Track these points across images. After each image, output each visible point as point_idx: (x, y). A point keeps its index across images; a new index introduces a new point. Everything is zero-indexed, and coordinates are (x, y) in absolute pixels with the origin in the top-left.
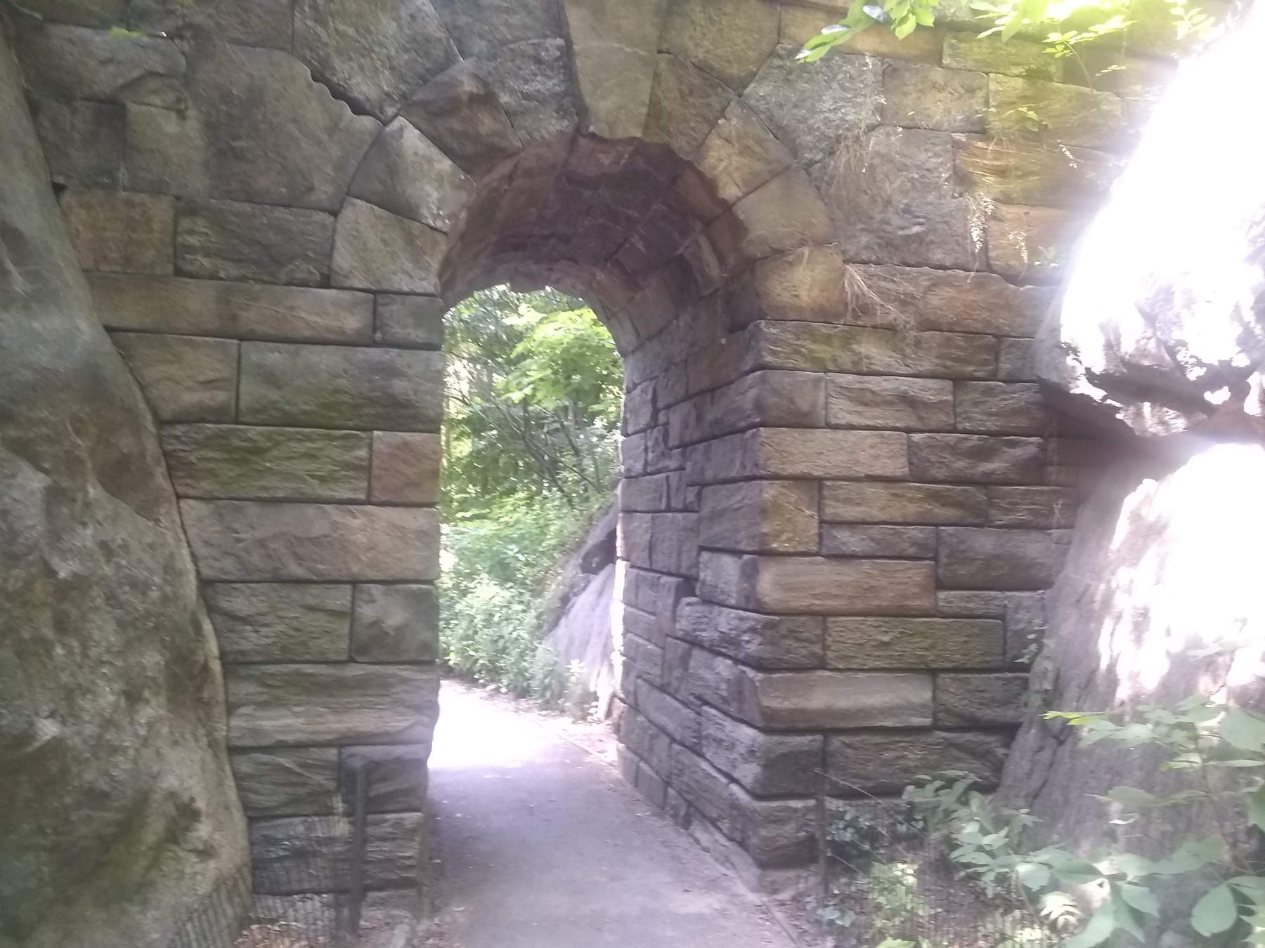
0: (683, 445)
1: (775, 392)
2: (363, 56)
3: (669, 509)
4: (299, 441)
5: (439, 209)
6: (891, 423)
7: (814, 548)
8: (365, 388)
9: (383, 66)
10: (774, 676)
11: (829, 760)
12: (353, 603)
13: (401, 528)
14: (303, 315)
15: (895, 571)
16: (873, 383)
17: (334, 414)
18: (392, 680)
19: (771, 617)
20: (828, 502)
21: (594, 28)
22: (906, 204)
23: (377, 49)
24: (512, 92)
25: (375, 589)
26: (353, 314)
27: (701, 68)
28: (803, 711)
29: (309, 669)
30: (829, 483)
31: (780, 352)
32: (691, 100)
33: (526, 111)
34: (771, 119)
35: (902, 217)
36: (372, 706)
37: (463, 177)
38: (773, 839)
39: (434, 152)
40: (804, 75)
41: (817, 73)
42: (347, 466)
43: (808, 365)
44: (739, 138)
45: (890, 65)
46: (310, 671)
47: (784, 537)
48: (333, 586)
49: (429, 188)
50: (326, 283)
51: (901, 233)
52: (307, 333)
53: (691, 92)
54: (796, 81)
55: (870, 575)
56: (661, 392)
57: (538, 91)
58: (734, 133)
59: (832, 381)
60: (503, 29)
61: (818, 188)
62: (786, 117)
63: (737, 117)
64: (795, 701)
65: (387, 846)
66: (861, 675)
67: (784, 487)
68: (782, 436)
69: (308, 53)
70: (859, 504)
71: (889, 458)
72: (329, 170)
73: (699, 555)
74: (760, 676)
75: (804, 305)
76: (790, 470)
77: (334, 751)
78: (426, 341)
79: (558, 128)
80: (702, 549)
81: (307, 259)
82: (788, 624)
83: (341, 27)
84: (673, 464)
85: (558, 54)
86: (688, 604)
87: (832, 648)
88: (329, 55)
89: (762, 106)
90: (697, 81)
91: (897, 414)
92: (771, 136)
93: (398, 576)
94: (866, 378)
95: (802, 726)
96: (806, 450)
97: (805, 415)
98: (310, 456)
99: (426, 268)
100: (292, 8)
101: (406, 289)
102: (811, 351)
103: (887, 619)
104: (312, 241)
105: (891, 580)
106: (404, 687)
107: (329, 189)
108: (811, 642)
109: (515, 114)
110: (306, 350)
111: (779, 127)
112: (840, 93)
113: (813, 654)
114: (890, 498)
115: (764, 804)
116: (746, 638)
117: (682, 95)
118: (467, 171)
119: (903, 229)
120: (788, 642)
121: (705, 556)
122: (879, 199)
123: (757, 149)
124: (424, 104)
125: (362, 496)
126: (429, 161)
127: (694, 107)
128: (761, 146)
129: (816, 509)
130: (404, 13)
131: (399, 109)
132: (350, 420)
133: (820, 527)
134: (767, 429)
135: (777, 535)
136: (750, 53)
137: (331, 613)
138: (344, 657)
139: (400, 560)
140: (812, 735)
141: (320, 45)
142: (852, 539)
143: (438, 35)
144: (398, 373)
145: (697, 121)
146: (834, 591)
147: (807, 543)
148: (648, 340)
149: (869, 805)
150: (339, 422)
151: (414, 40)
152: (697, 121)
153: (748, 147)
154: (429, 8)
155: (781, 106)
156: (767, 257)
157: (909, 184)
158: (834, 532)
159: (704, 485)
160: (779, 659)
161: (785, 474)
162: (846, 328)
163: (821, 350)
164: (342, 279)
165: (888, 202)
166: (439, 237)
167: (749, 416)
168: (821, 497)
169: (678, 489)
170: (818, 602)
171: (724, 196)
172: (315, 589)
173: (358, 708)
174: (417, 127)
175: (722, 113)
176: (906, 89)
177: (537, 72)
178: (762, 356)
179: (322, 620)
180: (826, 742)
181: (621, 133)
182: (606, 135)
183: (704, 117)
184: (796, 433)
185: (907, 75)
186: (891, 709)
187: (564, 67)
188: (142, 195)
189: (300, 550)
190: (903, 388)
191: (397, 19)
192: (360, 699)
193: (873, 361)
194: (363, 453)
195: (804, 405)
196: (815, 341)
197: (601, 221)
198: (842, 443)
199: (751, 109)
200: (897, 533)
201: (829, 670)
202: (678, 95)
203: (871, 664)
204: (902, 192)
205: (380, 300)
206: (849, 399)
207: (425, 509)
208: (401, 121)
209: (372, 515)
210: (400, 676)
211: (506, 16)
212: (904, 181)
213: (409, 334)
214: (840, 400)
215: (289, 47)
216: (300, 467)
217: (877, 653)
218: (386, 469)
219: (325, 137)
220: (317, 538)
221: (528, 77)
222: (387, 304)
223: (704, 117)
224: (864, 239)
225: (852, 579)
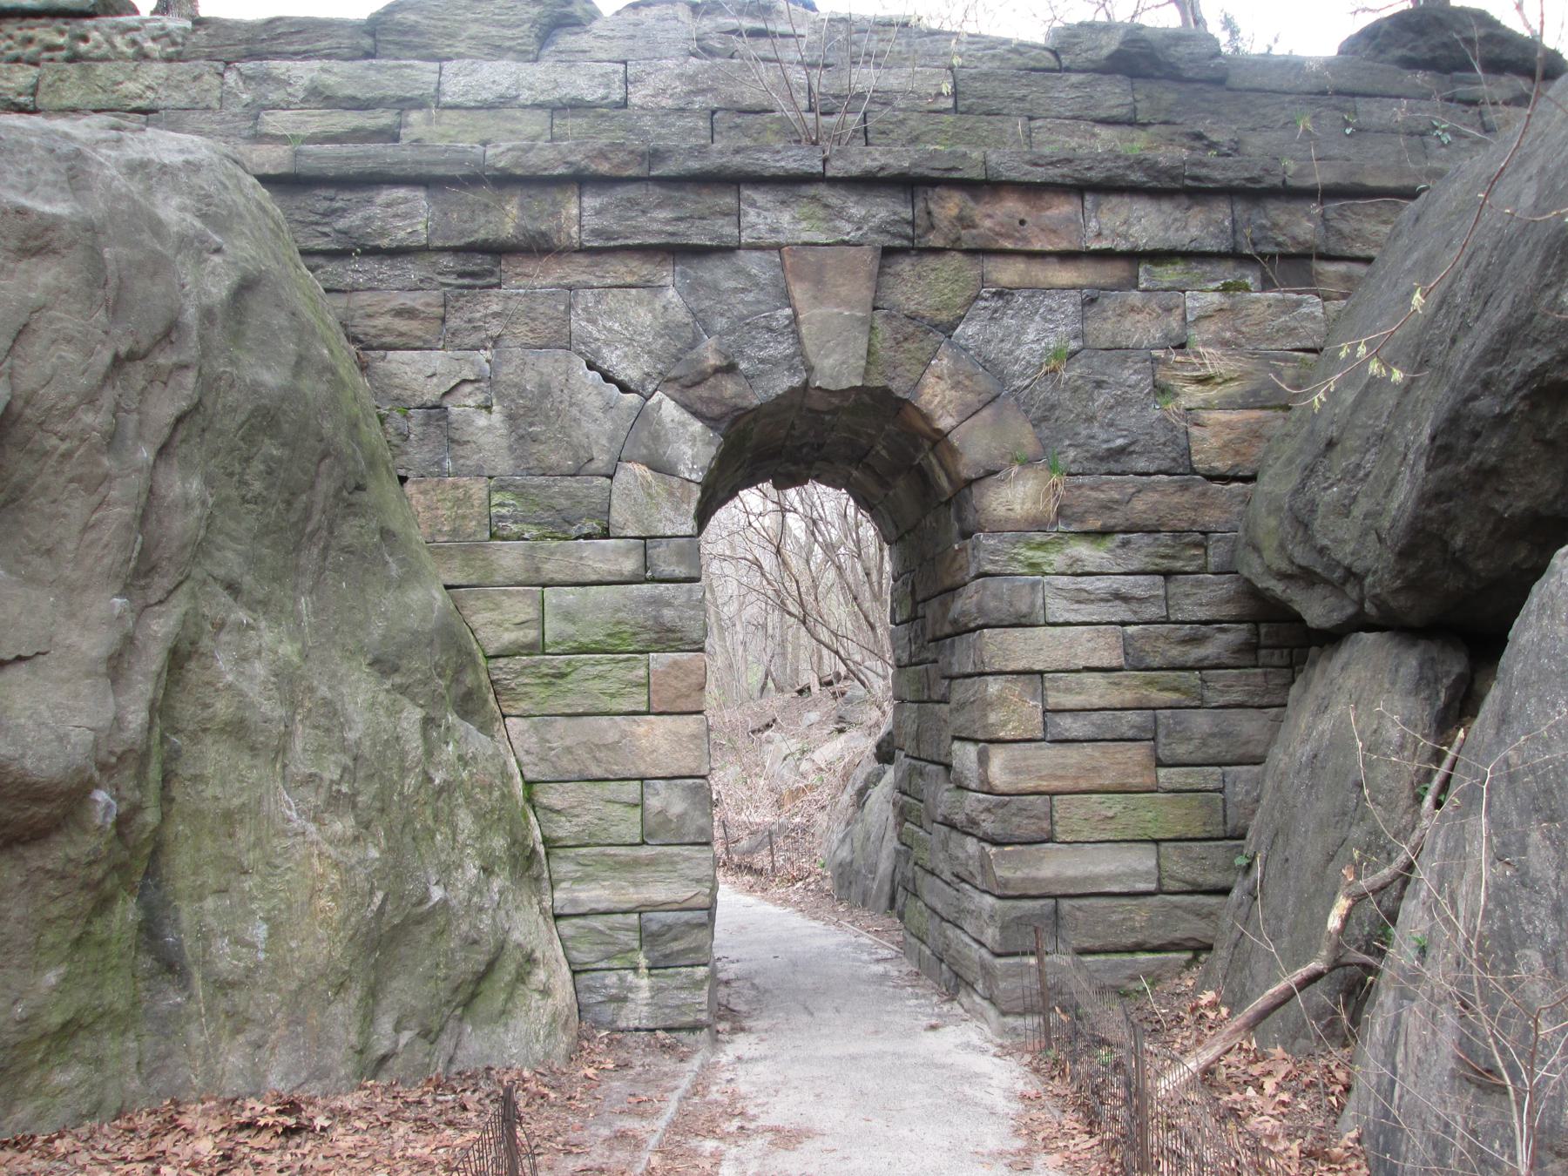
7: (1040, 735)
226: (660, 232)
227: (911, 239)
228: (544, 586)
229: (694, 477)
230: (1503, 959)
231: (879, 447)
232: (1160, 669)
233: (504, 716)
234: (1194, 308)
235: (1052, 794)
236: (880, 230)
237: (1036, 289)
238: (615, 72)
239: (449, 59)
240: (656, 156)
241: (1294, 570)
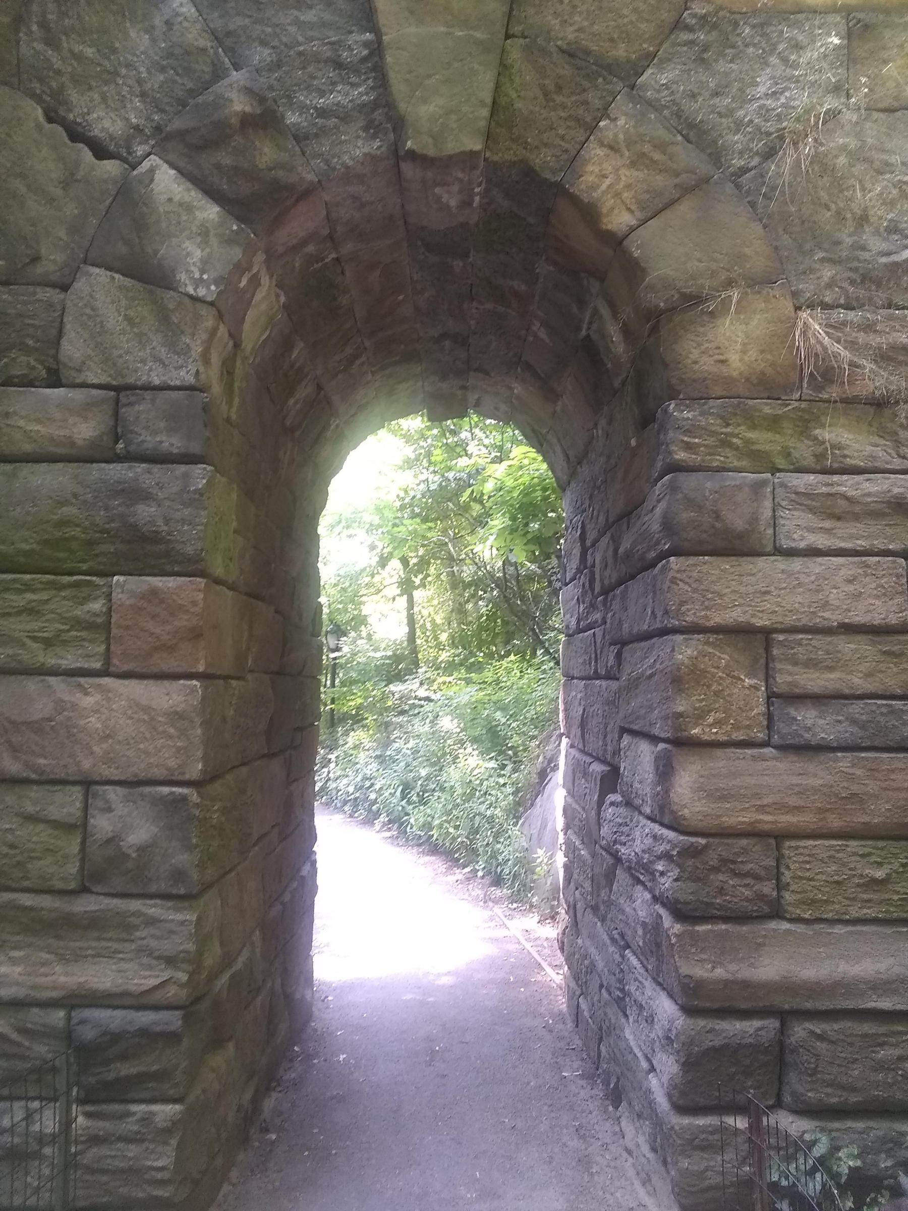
0: (606, 591)
1: (690, 503)
2: (106, 82)
3: (597, 676)
4: (20, 591)
5: (202, 272)
6: (879, 544)
7: (761, 736)
8: (100, 517)
9: (131, 93)
10: (698, 928)
11: (789, 1058)
12: (86, 808)
13: (147, 709)
14: (21, 423)
15: (893, 771)
16: (847, 485)
17: (62, 555)
18: (135, 921)
19: (693, 839)
20: (779, 666)
21: (412, 12)
22: (891, 220)
23: (124, 71)
24: (303, 108)
25: (114, 794)
26: (86, 419)
27: (570, 53)
28: (746, 984)
29: (27, 900)
30: (781, 637)
31: (698, 445)
32: (559, 99)
33: (323, 132)
34: (678, 115)
35: (884, 239)
36: (111, 955)
37: (235, 228)
38: (701, 1174)
39: (194, 196)
40: (727, 51)
41: (747, 46)
42: (78, 624)
43: (744, 463)
44: (629, 144)
45: (859, 21)
46: (28, 903)
48: (59, 787)
49: (188, 246)
50: (55, 379)
51: (884, 260)
52: (27, 447)
53: (559, 89)
54: (716, 61)
55: (850, 778)
56: (589, 527)
57: (338, 104)
58: (621, 136)
59: (782, 485)
60: (293, 29)
61: (752, 205)
62: (698, 110)
63: (626, 114)
64: (733, 967)
65: (132, 1150)
66: (839, 929)
67: (707, 643)
68: (705, 568)
69: (36, 85)
70: (830, 669)
71: (877, 597)
72: (62, 234)
73: (621, 737)
74: (678, 928)
75: (735, 374)
76: (717, 618)
77: (61, 1014)
78: (183, 450)
79: (366, 150)
80: (623, 731)
81: (25, 349)
82: (720, 850)
83: (77, 48)
84: (597, 616)
85: (365, 52)
86: (612, 804)
87: (793, 887)
88: (62, 86)
89: (664, 97)
90: (566, 71)
91: (889, 531)
92: (679, 138)
93: (142, 776)
94: (836, 478)
95: (744, 1005)
96: (742, 589)
97: (740, 536)
98: (31, 611)
99: (185, 352)
100: (17, 31)
101: (157, 381)
102: (747, 442)
103: (881, 844)
104: (33, 325)
105: (883, 785)
106: (152, 931)
107: (60, 257)
108: (757, 878)
109: (307, 137)
110: (26, 469)
111: (691, 126)
112: (780, 70)
113: (761, 897)
114: (879, 657)
115: (686, 1121)
116: (660, 867)
117: (546, 94)
118: (240, 219)
119: (888, 254)
120: (721, 877)
121: (626, 739)
122: (849, 216)
123: (657, 156)
124: (181, 134)
125: (97, 665)
126: (189, 208)
127: (564, 107)
128: (664, 153)
129: (762, 676)
130: (158, 21)
131: (153, 147)
132: (84, 561)
133: (769, 703)
134: (682, 559)
135: (699, 716)
136: (643, 26)
137: (56, 824)
138: (72, 885)
139: (147, 753)
140: (762, 1018)
141: (51, 74)
142: (821, 722)
143: (202, 43)
144: (146, 496)
145: (568, 127)
146: (793, 801)
147: (749, 727)
148: (578, 464)
149: (855, 1131)
150: (68, 566)
151: (170, 55)
152: (568, 127)
153: (644, 154)
154: (189, 10)
155: (693, 96)
156: (674, 309)
157: (895, 192)
158: (792, 711)
159: (624, 643)
160: (707, 904)
161: (711, 623)
162: (804, 405)
163: (763, 439)
164: (73, 374)
165: (863, 220)
166: (204, 311)
167: (658, 543)
168: (769, 658)
169: (602, 649)
171: (609, 227)
172: (34, 792)
173: (93, 956)
174: (172, 166)
175: (604, 113)
176: (885, 55)
177: (335, 79)
178: (670, 453)
179: (41, 835)
180: (783, 1030)
181: (451, 147)
182: (431, 152)
183: (577, 120)
184: (725, 564)
185: (888, 34)
186: (889, 982)
187: (375, 69)
189: (16, 739)
190: (896, 490)
191: (150, 30)
192: (94, 944)
193: (846, 452)
194: (97, 606)
195: (739, 523)
196: (753, 427)
197: (489, 306)
198: (802, 576)
199: (649, 103)
200: (892, 711)
201: (791, 920)
202: (539, 94)
203: (855, 912)
204: (884, 203)
205: (123, 400)
206: (811, 510)
207: (182, 682)
208: (154, 159)
209: (109, 691)
210: (145, 915)
211: (296, 13)
212: (886, 187)
213: (161, 442)
214: (795, 513)
215: (15, 80)
216: (18, 626)
217: (865, 896)
218: (128, 628)
219: (58, 192)
220: (37, 722)
221: (324, 87)
222: (131, 404)
223: (577, 120)
224: (827, 273)
225: (821, 782)
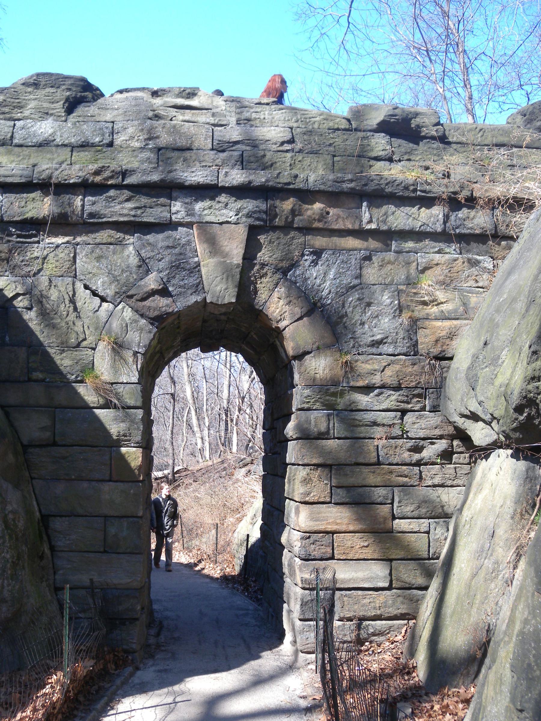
7: (328, 500)
47: (312, 495)
103: (366, 534)
170: (330, 527)
188: (15, 348)
226: (126, 215)
227: (265, 221)
228: (56, 408)
229: (140, 350)
230: (534, 648)
231: (252, 333)
232: (397, 464)
233: (32, 478)
234: (422, 263)
235: (333, 533)
236: (248, 216)
237: (337, 251)
238: (107, 128)
239: (19, 120)
240: (124, 174)
241: (469, 413)
